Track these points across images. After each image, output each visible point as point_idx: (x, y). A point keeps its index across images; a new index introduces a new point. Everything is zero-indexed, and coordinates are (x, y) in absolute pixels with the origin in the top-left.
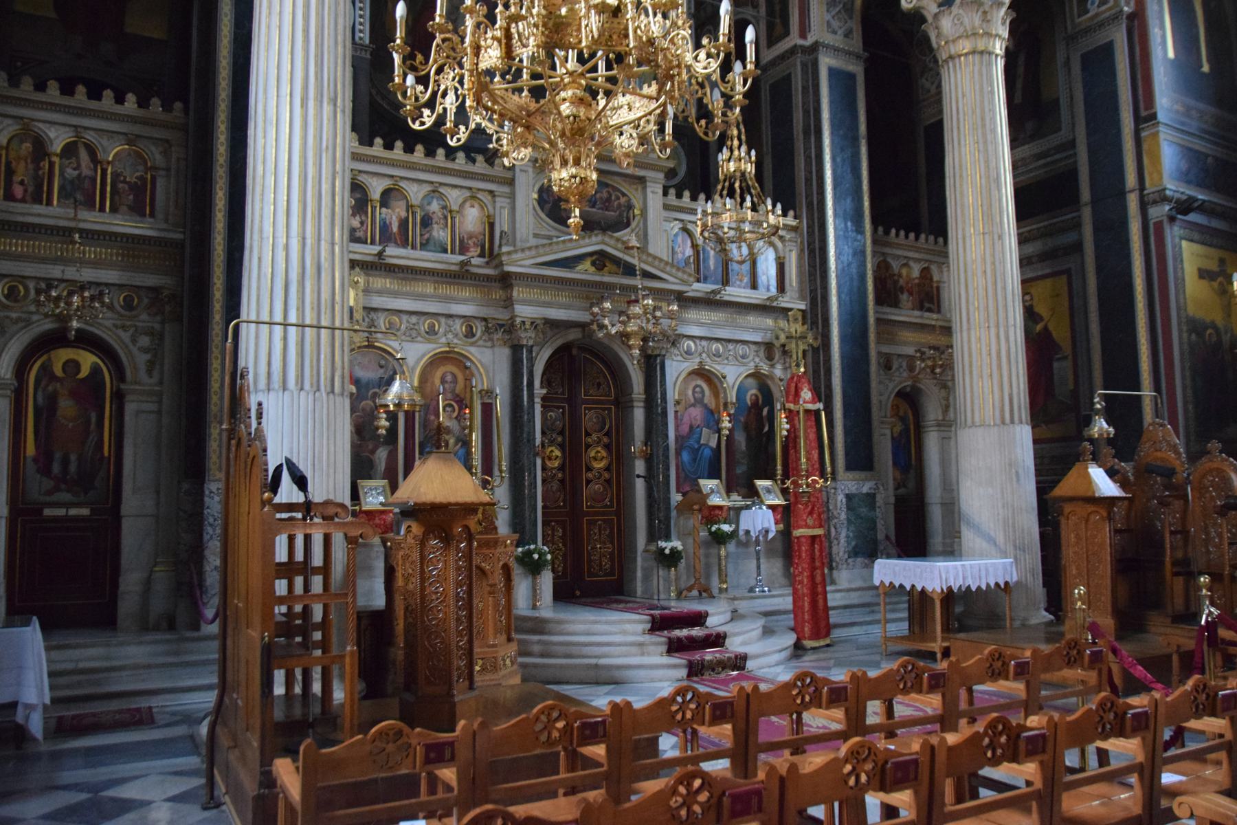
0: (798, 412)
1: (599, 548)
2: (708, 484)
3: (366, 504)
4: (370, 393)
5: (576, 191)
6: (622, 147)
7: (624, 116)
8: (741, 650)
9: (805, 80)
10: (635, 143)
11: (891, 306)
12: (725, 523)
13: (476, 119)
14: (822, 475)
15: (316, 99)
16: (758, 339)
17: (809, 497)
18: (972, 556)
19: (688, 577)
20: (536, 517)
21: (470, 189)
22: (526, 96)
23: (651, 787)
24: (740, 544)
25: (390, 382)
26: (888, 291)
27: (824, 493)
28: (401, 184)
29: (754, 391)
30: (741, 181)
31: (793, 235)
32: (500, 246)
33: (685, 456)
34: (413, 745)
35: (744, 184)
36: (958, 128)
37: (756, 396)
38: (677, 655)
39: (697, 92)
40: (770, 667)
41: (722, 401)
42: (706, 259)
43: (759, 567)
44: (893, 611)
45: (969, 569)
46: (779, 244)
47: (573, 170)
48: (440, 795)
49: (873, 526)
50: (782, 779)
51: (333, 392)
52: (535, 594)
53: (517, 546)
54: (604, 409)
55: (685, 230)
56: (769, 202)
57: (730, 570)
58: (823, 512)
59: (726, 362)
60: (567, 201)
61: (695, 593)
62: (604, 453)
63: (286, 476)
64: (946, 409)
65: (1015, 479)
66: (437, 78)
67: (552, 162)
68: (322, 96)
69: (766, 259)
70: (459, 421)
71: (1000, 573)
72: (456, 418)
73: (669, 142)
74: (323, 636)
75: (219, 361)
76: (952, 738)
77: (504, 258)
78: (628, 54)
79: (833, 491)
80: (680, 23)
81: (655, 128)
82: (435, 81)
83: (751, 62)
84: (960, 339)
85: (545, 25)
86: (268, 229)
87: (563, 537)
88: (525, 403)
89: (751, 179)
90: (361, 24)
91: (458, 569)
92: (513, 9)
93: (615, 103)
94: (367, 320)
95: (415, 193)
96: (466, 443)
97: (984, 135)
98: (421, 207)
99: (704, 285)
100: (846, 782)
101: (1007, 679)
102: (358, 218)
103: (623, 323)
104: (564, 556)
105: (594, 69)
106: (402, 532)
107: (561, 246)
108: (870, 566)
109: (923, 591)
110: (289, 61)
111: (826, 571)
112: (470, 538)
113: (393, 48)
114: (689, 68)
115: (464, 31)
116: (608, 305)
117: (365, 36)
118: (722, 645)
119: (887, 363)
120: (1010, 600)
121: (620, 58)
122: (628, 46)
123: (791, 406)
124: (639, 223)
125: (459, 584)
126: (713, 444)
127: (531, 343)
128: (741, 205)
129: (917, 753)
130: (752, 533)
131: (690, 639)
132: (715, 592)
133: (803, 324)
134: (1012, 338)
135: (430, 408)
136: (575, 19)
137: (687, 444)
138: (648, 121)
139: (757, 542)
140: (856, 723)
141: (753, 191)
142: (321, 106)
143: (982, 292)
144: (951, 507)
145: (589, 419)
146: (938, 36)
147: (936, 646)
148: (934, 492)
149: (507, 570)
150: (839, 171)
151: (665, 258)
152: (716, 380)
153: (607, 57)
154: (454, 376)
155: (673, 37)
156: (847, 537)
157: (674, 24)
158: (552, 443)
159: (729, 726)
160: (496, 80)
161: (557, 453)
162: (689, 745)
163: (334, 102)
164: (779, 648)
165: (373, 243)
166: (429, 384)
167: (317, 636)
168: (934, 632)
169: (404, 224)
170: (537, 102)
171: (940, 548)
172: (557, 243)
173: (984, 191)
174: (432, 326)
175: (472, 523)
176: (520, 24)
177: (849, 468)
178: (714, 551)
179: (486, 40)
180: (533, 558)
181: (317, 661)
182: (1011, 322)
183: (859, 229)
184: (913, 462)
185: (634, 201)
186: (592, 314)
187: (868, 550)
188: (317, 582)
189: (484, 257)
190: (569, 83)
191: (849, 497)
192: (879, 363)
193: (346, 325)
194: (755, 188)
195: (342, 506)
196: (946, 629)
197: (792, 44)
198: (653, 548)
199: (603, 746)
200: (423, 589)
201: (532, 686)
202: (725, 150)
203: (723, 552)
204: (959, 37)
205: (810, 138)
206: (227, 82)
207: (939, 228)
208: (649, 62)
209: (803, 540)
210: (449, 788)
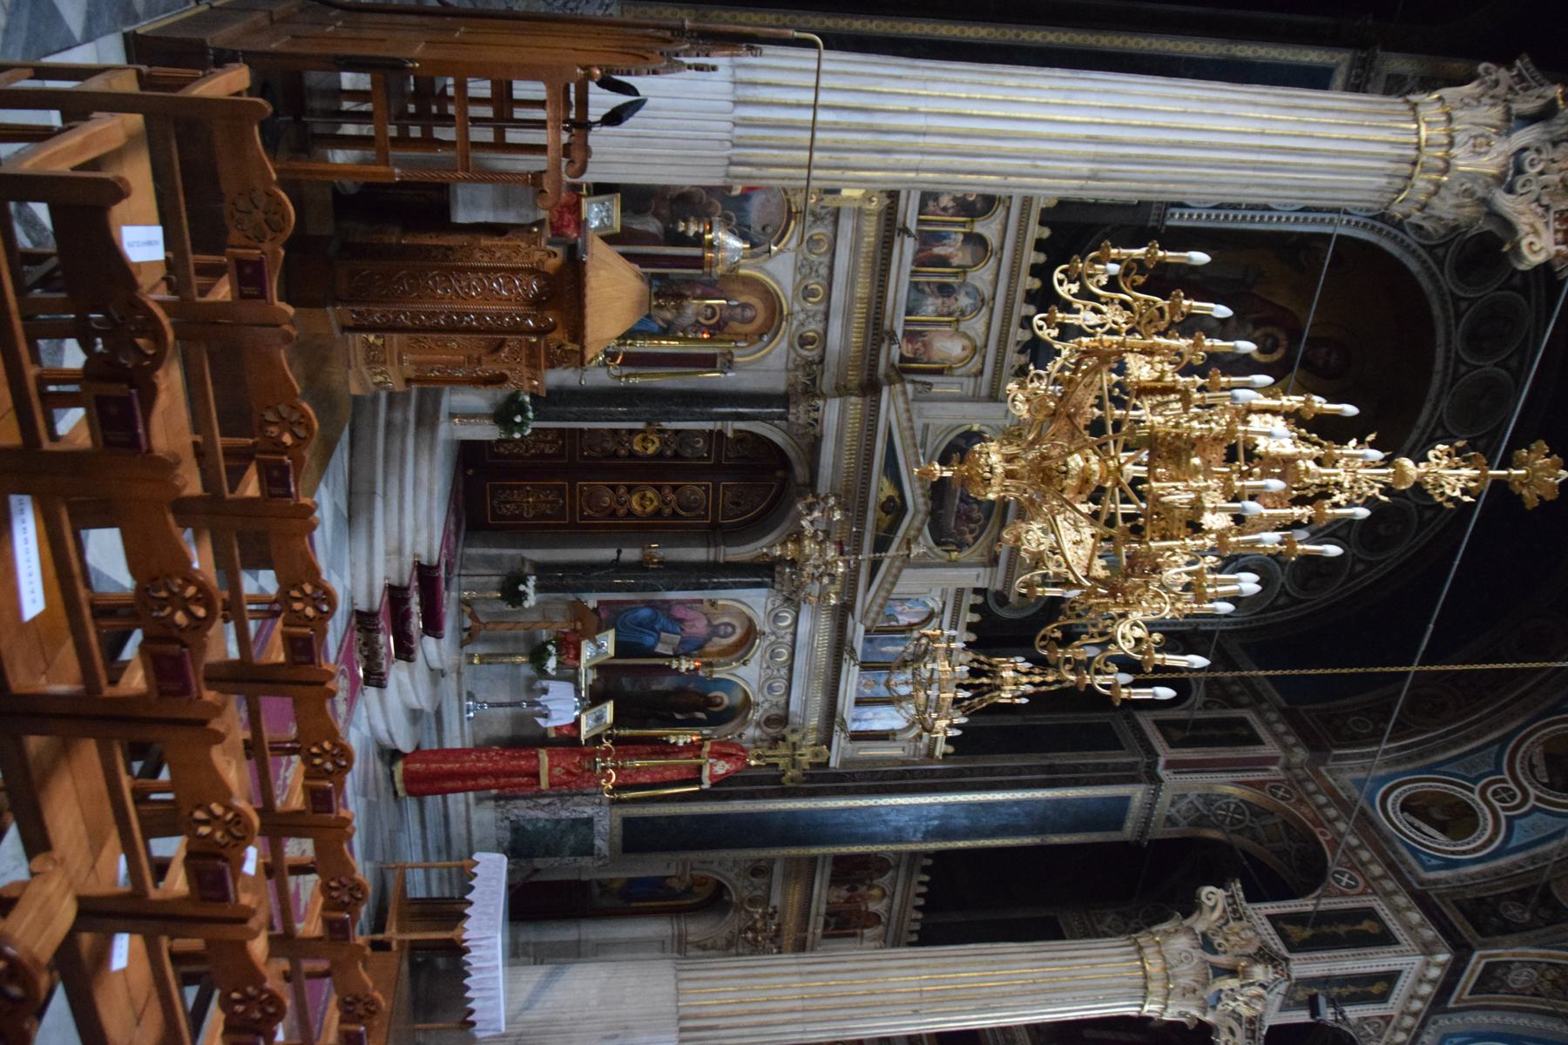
0: (698, 757)
1: (529, 500)
2: (608, 641)
3: (590, 204)
4: (732, 214)
5: (973, 472)
6: (1027, 532)
7: (1067, 535)
8: (391, 681)
9: (1117, 767)
10: (1033, 547)
11: (832, 875)
12: (558, 662)
14: (618, 788)
15: (1096, 154)
16: (792, 708)
17: (589, 770)
18: (511, 980)
19: (486, 614)
20: (569, 420)
21: (986, 346)
22: (1093, 414)
23: (200, 559)
24: (531, 681)
25: (743, 237)
26: (851, 871)
27: (594, 790)
28: (992, 260)
29: (726, 701)
30: (989, 685)
31: (923, 752)
32: (913, 382)
33: (645, 613)
34: (260, 245)
35: (985, 689)
36: (1053, 959)
37: (721, 704)
38: (386, 598)
39: (1094, 626)
40: (369, 718)
41: (715, 660)
42: (893, 642)
43: (500, 705)
44: (441, 879)
45: (493, 975)
47: (999, 470)
48: (196, 281)
49: (549, 853)
50: (204, 723)
51: (732, 163)
52: (469, 416)
53: (532, 396)
54: (706, 509)
55: (931, 615)
56: (964, 720)
57: (495, 668)
58: (570, 789)
59: (765, 665)
60: (961, 462)
61: (468, 623)
62: (649, 509)
63: (621, 99)
64: (702, 946)
65: (609, 1033)
66: (1116, 301)
67: (1010, 443)
69: (893, 718)
70: (693, 325)
71: (487, 1016)
72: (697, 322)
74: (415, 140)
75: (774, 23)
76: (259, 947)
77: (898, 387)
79: (597, 801)
80: (1179, 605)
81: (1051, 573)
82: (1112, 299)
84: (788, 963)
85: (1178, 436)
86: (936, 89)
87: (542, 455)
88: (715, 410)
89: (992, 698)
90: (1190, 216)
91: (500, 316)
92: (1197, 396)
93: (1084, 523)
94: (824, 211)
95: (981, 277)
96: (666, 332)
97: (1043, 991)
98: (964, 284)
99: (861, 639)
100: (198, 807)
101: (342, 1021)
102: (951, 204)
103: (815, 535)
104: (518, 456)
105: (1126, 500)
106: (550, 248)
107: (912, 459)
108: (499, 848)
109: (465, 917)
110: (1143, 123)
111: (494, 792)
112: (539, 332)
113: (1153, 247)
114: (1124, 616)
116: (837, 516)
117: (1175, 220)
118: (398, 657)
119: (760, 870)
120: (449, 1029)
121: (1137, 531)
122: (1152, 539)
123: (707, 749)
125: (480, 316)
126: (660, 649)
127: (791, 418)
128: (959, 686)
129: (237, 900)
130: (543, 697)
131: (407, 615)
132: (469, 649)
133: (811, 764)
134: (788, 1029)
135: (712, 288)
136: (1184, 474)
137: (660, 613)
138: (1059, 566)
139: (533, 704)
140: (277, 826)
141: (976, 700)
142: (1088, 161)
143: (846, 990)
144: (576, 953)
145: (695, 490)
146: (1167, 933)
147: (392, 933)
148: (594, 931)
149: (498, 380)
150: (1002, 810)
152: (740, 653)
153: (1140, 516)
154: (751, 320)
155: (1162, 597)
156: (538, 819)
157: (1178, 598)
158: (664, 443)
159: (282, 658)
160: (1114, 376)
161: (651, 450)
162: (265, 607)
163: (1094, 177)
164: (394, 730)
165: (920, 222)
166: (741, 288)
167: (415, 132)
168: (411, 931)
169: (943, 261)
170: (1086, 427)
171: (523, 938)
172: (917, 455)
173: (973, 991)
174: (814, 294)
175: (558, 336)
176: (1179, 405)
177: (628, 822)
178: (522, 647)
179: (1161, 362)
180: (515, 415)
181: (381, 130)
182: (810, 1028)
183: (929, 835)
184: (634, 904)
185: (967, 552)
186: (827, 497)
187: (520, 846)
188: (485, 135)
189: (901, 361)
190: (1108, 467)
191: (589, 822)
192: (760, 860)
193: (813, 183)
194: (981, 702)
195: (583, 170)
196: (415, 946)
197: (1159, 750)
198: (527, 569)
199: (258, 494)
200: (475, 270)
201: (346, 411)
202: (1029, 665)
203: (520, 659)
204: (1164, 959)
207: (929, 936)
208: (1131, 565)
209: (534, 763)
210: (203, 293)
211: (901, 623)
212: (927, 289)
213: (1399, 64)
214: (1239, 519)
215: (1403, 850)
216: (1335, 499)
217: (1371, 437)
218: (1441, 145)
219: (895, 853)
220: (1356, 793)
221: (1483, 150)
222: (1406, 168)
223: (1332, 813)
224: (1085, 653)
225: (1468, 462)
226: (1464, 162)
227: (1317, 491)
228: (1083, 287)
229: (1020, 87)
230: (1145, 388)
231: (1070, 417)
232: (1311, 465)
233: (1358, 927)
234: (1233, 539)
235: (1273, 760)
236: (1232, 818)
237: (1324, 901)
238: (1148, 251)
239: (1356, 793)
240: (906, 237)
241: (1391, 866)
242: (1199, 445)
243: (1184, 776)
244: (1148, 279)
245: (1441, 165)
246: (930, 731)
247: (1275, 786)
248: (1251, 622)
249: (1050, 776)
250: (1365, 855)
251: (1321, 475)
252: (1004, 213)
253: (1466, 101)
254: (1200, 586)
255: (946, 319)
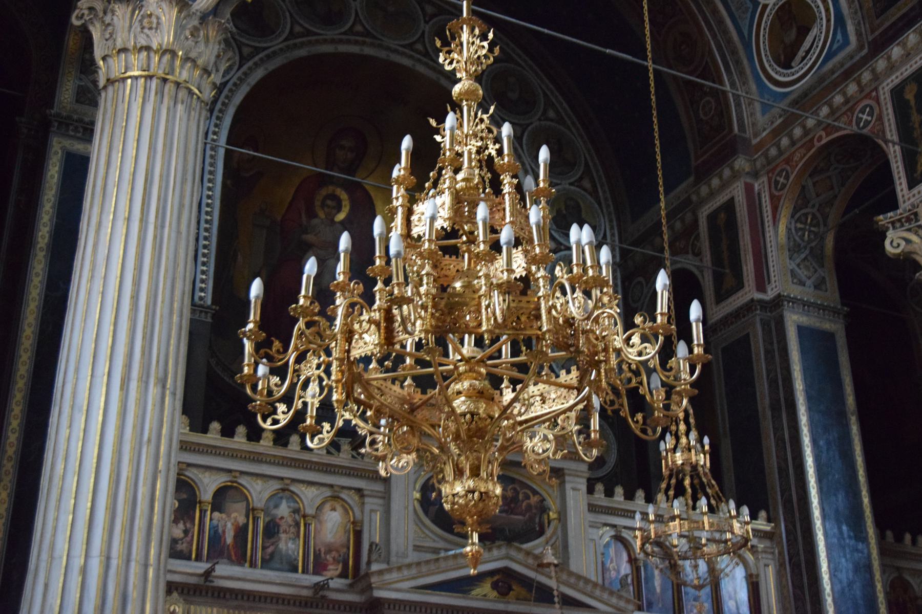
5: (474, 510)
9: (768, 341)
13: (344, 416)
15: (140, 379)
21: (331, 486)
22: (410, 386)
30: (692, 477)
32: (369, 563)
35: (696, 481)
39: (630, 380)
46: (749, 556)
47: (471, 483)
55: (618, 538)
56: (732, 504)
60: (463, 523)
66: (297, 367)
68: (148, 377)
73: (595, 441)
77: (373, 579)
78: (539, 339)
80: (606, 299)
82: (295, 371)
83: (698, 345)
86: (62, 546)
89: (705, 474)
90: (203, 281)
98: (266, 511)
102: (181, 525)
107: (451, 563)
115: (334, 311)
122: (540, 329)
124: (556, 529)
141: (709, 491)
151: (593, 578)
155: (598, 316)
165: (198, 558)
169: (241, 533)
170: (424, 392)
172: (446, 558)
176: (405, 307)
179: (361, 322)
189: (346, 577)
190: (466, 372)
194: (712, 487)
197: (747, 298)
205: (780, 416)
206: (29, 354)
208: (566, 347)
211: (628, 571)
212: (270, 550)
213: (66, 94)
214: (517, 243)
215: (830, 65)
216: (494, 153)
217: (433, 123)
218: (149, 57)
219: (883, 572)
220: (775, 111)
221: (154, 20)
222: (169, 87)
223: (798, 132)
224: (657, 388)
225: (455, 35)
226: (165, 37)
227: (485, 170)
228: (281, 400)
229: (66, 459)
230: (386, 339)
231: (413, 409)
232: (460, 176)
233: (912, 103)
234: (538, 250)
235: (749, 189)
236: (811, 225)
237: (889, 136)
238: (248, 338)
239: (775, 111)
240: (213, 574)
241: (847, 75)
242: (442, 281)
243: (772, 274)
244: (277, 338)
245: (167, 57)
246: (747, 540)
247: (774, 185)
248: (609, 214)
249: (783, 408)
250: (838, 99)
251: (470, 167)
252: (195, 471)
253: (108, 36)
254: (586, 282)
255: (302, 528)
